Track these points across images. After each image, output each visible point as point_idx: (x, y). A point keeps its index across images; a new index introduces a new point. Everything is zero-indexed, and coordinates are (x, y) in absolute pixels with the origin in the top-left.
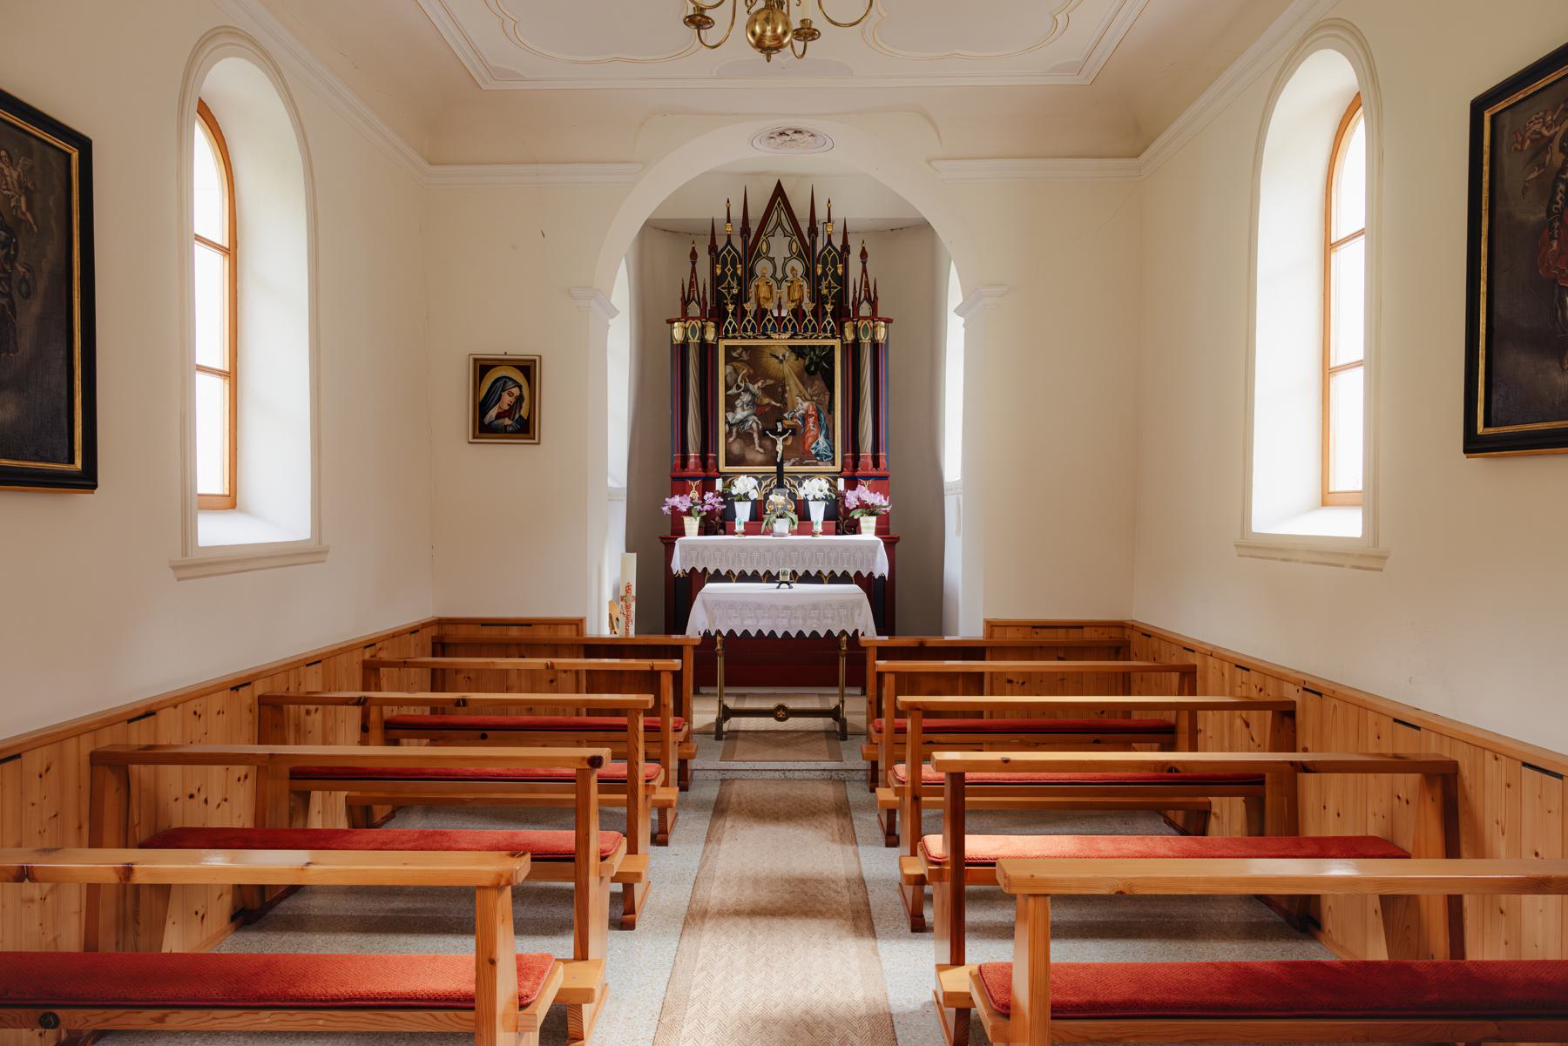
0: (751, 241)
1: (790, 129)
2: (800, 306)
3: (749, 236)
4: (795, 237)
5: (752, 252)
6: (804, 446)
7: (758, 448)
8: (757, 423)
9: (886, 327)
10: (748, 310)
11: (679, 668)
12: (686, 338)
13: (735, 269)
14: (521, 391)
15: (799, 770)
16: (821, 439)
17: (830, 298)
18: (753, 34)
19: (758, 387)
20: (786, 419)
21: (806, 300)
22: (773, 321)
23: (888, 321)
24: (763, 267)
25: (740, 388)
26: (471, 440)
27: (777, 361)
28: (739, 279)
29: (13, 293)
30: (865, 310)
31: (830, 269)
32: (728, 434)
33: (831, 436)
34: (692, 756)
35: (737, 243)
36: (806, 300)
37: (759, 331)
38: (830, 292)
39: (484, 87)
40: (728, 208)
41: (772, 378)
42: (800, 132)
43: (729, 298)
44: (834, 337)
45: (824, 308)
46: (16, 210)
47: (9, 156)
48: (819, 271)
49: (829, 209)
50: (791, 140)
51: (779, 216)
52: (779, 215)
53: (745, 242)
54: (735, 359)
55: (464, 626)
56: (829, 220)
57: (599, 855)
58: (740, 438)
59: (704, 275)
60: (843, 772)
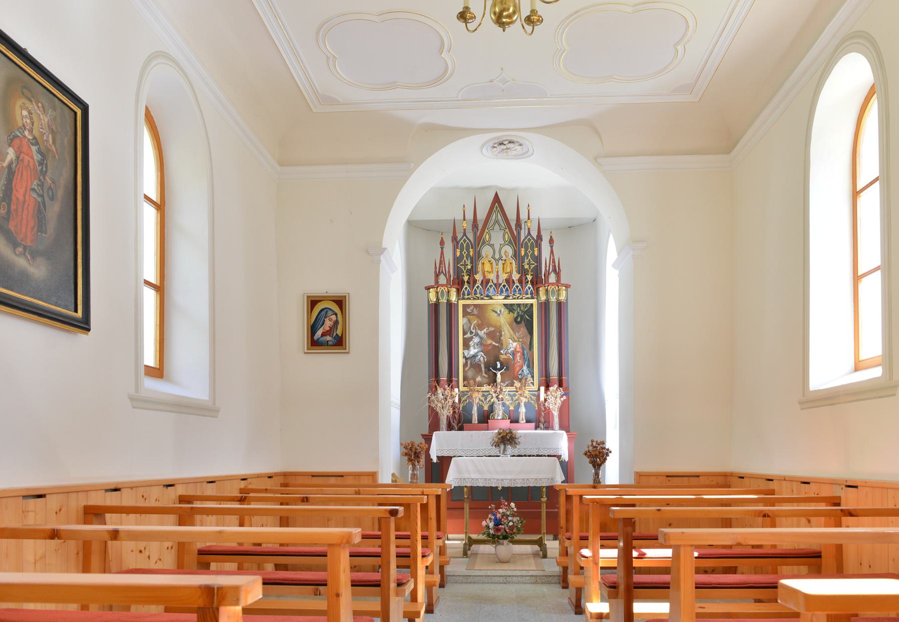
0: (478, 233)
1: (506, 140)
2: (511, 276)
4: (507, 230)
5: (479, 241)
6: (514, 373)
7: (484, 374)
8: (484, 357)
9: (567, 291)
10: (477, 279)
12: (438, 299)
13: (469, 252)
14: (337, 317)
15: (515, 576)
16: (525, 368)
17: (530, 271)
18: (495, 13)
19: (484, 332)
21: (514, 272)
22: (494, 286)
24: (486, 251)
25: (473, 333)
26: (306, 351)
27: (496, 314)
28: (472, 259)
29: (44, 195)
30: (552, 278)
32: (465, 365)
33: (531, 366)
34: (448, 563)
35: (471, 236)
36: (514, 272)
38: (530, 267)
40: (464, 211)
41: (492, 327)
42: (513, 142)
43: (465, 272)
44: (533, 298)
45: (526, 278)
46: (47, 143)
47: (43, 107)
48: (523, 253)
49: (529, 210)
50: (507, 149)
51: (497, 216)
52: (496, 216)
53: (475, 234)
54: (469, 314)
55: (300, 477)
56: (529, 219)
57: (396, 581)
59: (449, 257)
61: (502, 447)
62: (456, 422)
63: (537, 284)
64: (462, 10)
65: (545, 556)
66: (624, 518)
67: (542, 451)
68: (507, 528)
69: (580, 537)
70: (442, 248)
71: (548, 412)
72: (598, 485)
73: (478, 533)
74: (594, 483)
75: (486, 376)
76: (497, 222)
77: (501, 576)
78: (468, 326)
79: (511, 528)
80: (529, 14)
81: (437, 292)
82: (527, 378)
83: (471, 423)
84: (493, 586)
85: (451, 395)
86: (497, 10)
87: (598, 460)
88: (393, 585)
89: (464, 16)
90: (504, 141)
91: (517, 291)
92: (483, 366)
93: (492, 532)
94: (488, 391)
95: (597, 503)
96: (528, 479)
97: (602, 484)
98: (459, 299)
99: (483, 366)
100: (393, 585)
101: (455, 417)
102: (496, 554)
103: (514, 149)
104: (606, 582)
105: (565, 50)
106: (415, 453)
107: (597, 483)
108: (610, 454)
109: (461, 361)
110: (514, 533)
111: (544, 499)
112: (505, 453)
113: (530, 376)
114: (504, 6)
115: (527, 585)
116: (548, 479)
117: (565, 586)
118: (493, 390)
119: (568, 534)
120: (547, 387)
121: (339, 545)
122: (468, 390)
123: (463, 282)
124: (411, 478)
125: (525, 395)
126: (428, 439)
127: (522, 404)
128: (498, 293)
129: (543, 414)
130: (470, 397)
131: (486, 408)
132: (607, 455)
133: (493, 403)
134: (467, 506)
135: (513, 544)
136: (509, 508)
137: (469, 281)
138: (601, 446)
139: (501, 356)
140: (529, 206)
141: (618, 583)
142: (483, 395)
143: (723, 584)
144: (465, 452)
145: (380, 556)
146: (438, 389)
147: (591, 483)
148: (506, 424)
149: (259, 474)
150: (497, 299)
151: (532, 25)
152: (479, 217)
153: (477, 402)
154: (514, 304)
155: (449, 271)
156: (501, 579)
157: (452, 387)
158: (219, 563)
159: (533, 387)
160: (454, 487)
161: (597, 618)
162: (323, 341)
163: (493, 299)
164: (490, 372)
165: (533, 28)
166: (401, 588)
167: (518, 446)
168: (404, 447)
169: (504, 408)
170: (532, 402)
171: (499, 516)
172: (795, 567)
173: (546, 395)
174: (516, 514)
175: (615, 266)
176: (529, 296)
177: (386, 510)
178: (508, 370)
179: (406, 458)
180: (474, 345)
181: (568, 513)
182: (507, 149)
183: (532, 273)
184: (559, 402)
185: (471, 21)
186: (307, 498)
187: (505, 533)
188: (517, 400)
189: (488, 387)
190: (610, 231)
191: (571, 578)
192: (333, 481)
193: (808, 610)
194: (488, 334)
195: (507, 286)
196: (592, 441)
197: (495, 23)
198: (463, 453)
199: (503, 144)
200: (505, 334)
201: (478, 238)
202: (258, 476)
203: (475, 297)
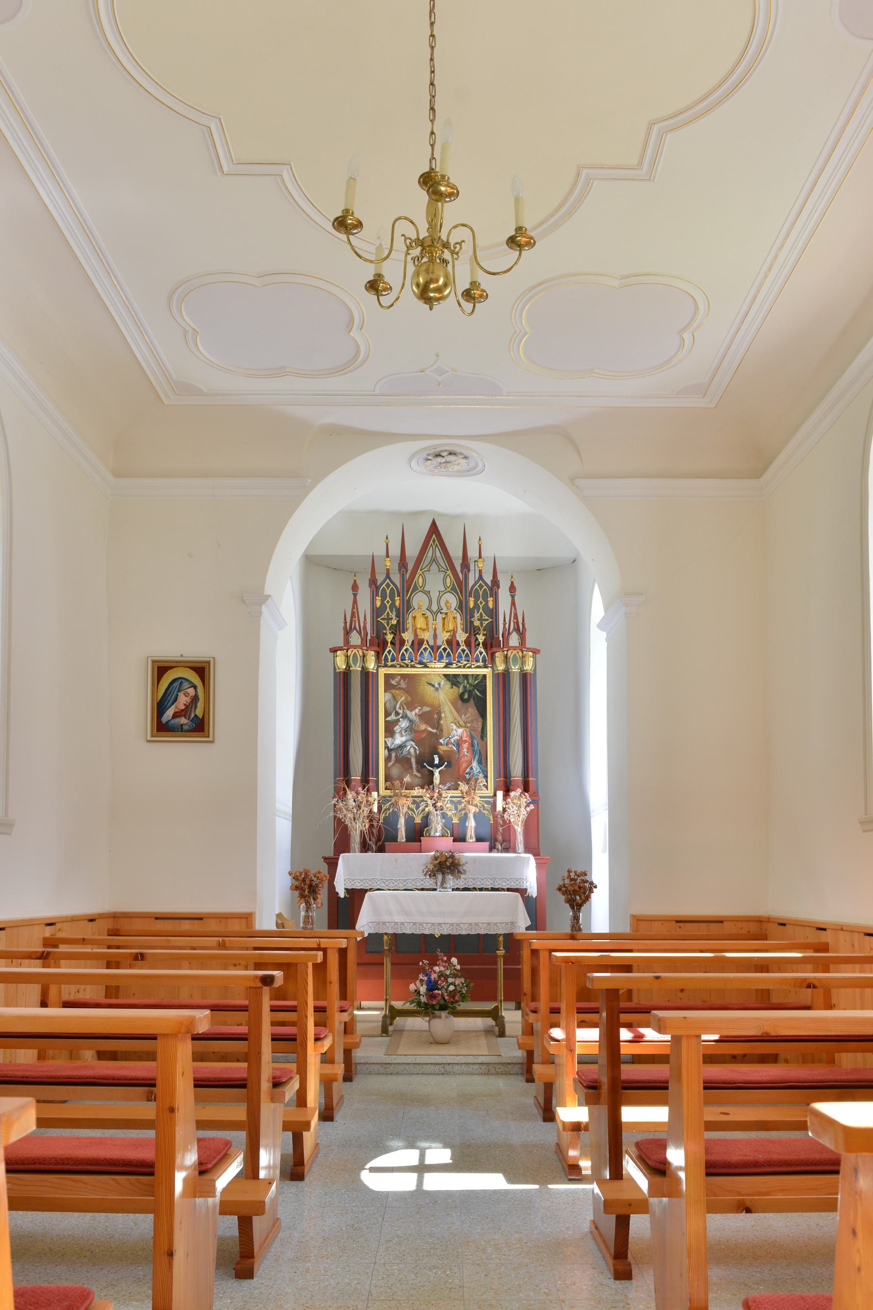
1: (445, 451)
3: (407, 571)
4: (449, 572)
5: (408, 586)
6: (459, 772)
7: (415, 773)
9: (534, 658)
11: (344, 946)
12: (348, 666)
13: (394, 601)
14: (196, 691)
15: (458, 1064)
16: (475, 764)
17: (482, 629)
18: (418, 285)
19: (416, 714)
20: (441, 744)
21: (460, 631)
22: (429, 649)
23: (535, 652)
24: (419, 600)
26: (149, 738)
27: (433, 688)
28: (398, 611)
30: (514, 640)
31: (481, 603)
32: (388, 759)
33: (483, 761)
34: (357, 1045)
35: (396, 578)
36: (460, 631)
37: (416, 660)
39: (166, 402)
40: (387, 545)
41: (428, 705)
42: (455, 454)
43: (388, 628)
44: (485, 667)
45: (477, 639)
48: (472, 605)
49: (480, 546)
50: (447, 462)
51: (434, 552)
54: (394, 687)
56: (480, 557)
57: (271, 1080)
58: (399, 763)
60: (500, 1066)
61: (440, 877)
62: (374, 840)
63: (492, 647)
64: (372, 278)
65: (502, 1034)
66: (606, 990)
67: (500, 882)
68: (446, 994)
69: (551, 1009)
70: (355, 595)
71: (508, 827)
72: (578, 933)
73: (404, 999)
74: (572, 930)
75: (418, 775)
76: (434, 560)
77: (437, 1064)
78: (393, 705)
79: (452, 994)
80: (468, 287)
81: (347, 656)
82: (478, 779)
83: (396, 841)
84: (423, 1079)
85: (367, 801)
86: (421, 280)
87: (578, 898)
88: (265, 1085)
89: (374, 286)
90: (442, 451)
91: (463, 656)
92: (413, 760)
93: (423, 999)
94: (421, 797)
95: (572, 963)
96: (477, 924)
97: (583, 932)
98: (379, 667)
99: (413, 760)
100: (265, 1085)
101: (372, 833)
102: (429, 1031)
103: (457, 462)
104: (583, 1080)
105: (525, 334)
106: (310, 886)
107: (576, 932)
108: (594, 889)
109: (382, 753)
110: (457, 1002)
111: (501, 952)
112: (445, 886)
113: (481, 775)
114: (431, 276)
115: (475, 1077)
116: (507, 924)
117: (530, 1080)
118: (428, 795)
119: (533, 1005)
120: (506, 795)
121: (174, 1035)
122: (392, 794)
123: (385, 643)
124: (304, 922)
125: (475, 802)
126: (333, 863)
127: (471, 815)
128: (435, 659)
129: (501, 829)
130: (395, 804)
131: (418, 820)
132: (591, 891)
133: (429, 813)
134: (387, 962)
135: (454, 1016)
136: (449, 965)
137: (393, 641)
138: (582, 878)
139: (440, 747)
140: (480, 540)
141: (600, 1082)
142: (414, 802)
143: (752, 1083)
144: (387, 883)
145: (246, 1039)
146: (348, 792)
147: (568, 930)
148: (446, 844)
149: (74, 916)
150: (435, 668)
151: (473, 301)
152: (408, 553)
153: (404, 811)
154: (459, 675)
155: (365, 628)
156: (437, 1069)
157: (368, 790)
158: (8, 1050)
159: (487, 792)
160: (369, 934)
161: (573, 1130)
162: (174, 724)
163: (429, 667)
164: (424, 769)
165: (474, 306)
166: (277, 1090)
167: (462, 876)
168: (294, 878)
169: (444, 821)
170: (486, 812)
171: (434, 976)
172: (859, 1055)
173: (505, 802)
174: (460, 974)
175: (601, 626)
176: (481, 664)
177: (256, 977)
178: (451, 767)
179: (297, 893)
180: (401, 731)
181: (535, 972)
182: (447, 462)
183: (485, 633)
184: (524, 813)
185: (386, 293)
186: (142, 954)
187: (442, 1002)
188: (464, 809)
189: (420, 790)
190: (594, 580)
191: (537, 1068)
192: (186, 926)
193: (849, 1150)
194: (422, 716)
195: (449, 650)
196: (569, 871)
197: (419, 299)
198: (384, 885)
199: (440, 455)
200: (445, 716)
201: (407, 581)
202: (73, 920)
203: (402, 664)
